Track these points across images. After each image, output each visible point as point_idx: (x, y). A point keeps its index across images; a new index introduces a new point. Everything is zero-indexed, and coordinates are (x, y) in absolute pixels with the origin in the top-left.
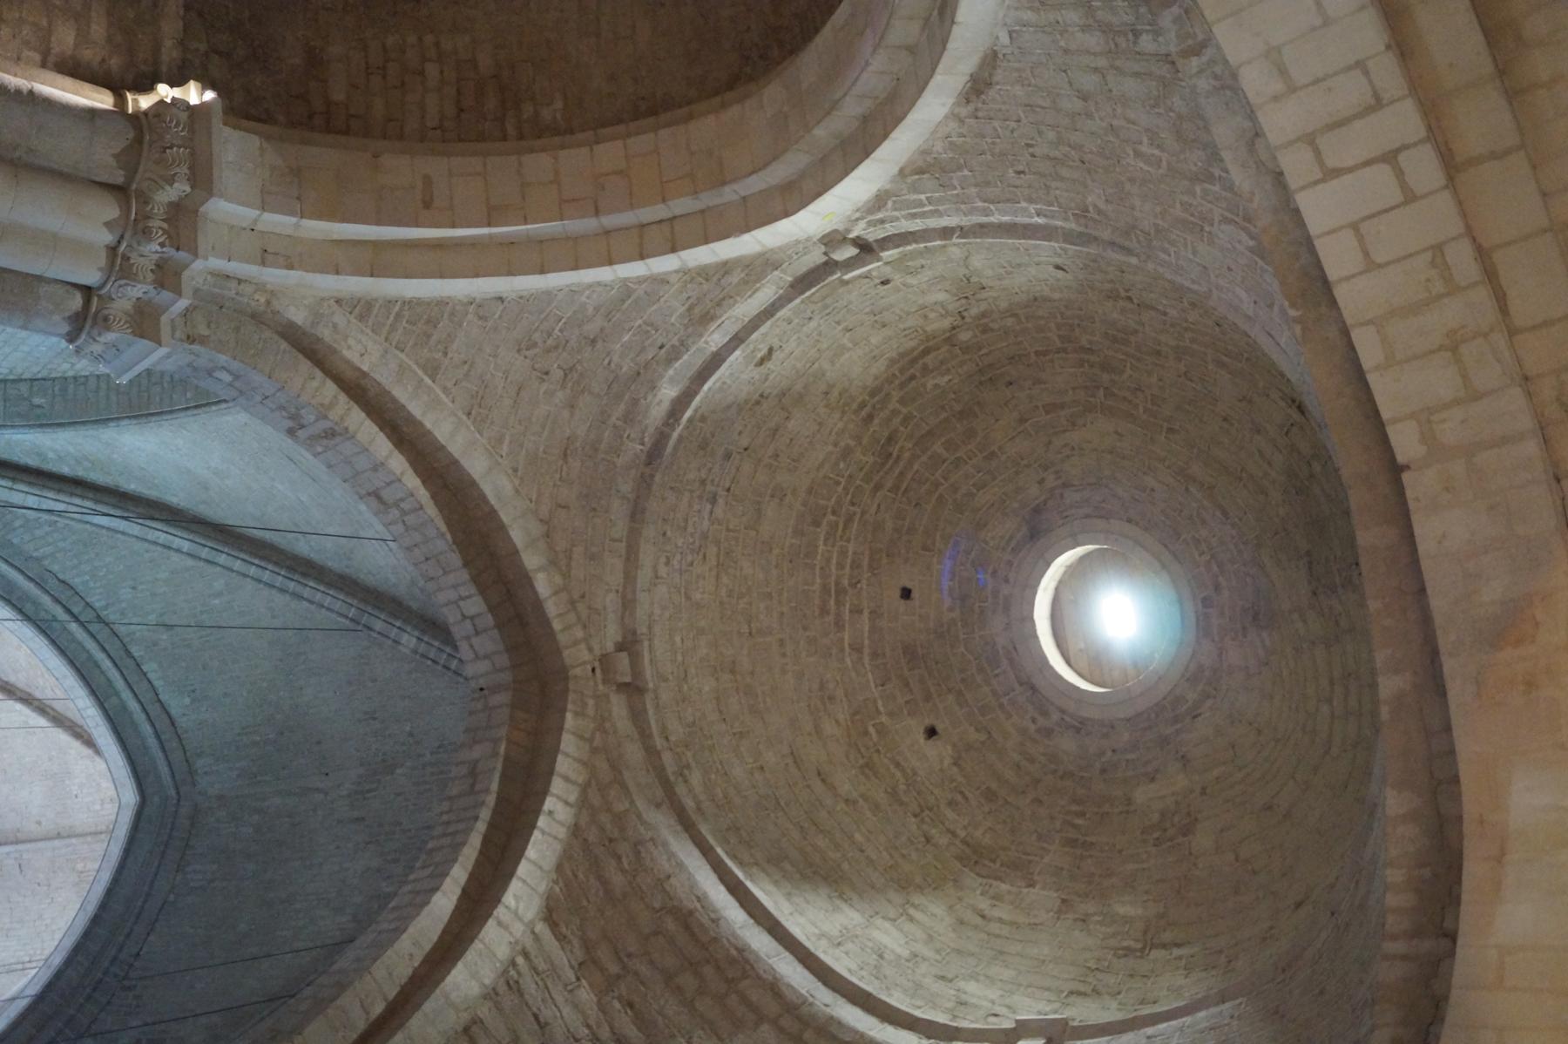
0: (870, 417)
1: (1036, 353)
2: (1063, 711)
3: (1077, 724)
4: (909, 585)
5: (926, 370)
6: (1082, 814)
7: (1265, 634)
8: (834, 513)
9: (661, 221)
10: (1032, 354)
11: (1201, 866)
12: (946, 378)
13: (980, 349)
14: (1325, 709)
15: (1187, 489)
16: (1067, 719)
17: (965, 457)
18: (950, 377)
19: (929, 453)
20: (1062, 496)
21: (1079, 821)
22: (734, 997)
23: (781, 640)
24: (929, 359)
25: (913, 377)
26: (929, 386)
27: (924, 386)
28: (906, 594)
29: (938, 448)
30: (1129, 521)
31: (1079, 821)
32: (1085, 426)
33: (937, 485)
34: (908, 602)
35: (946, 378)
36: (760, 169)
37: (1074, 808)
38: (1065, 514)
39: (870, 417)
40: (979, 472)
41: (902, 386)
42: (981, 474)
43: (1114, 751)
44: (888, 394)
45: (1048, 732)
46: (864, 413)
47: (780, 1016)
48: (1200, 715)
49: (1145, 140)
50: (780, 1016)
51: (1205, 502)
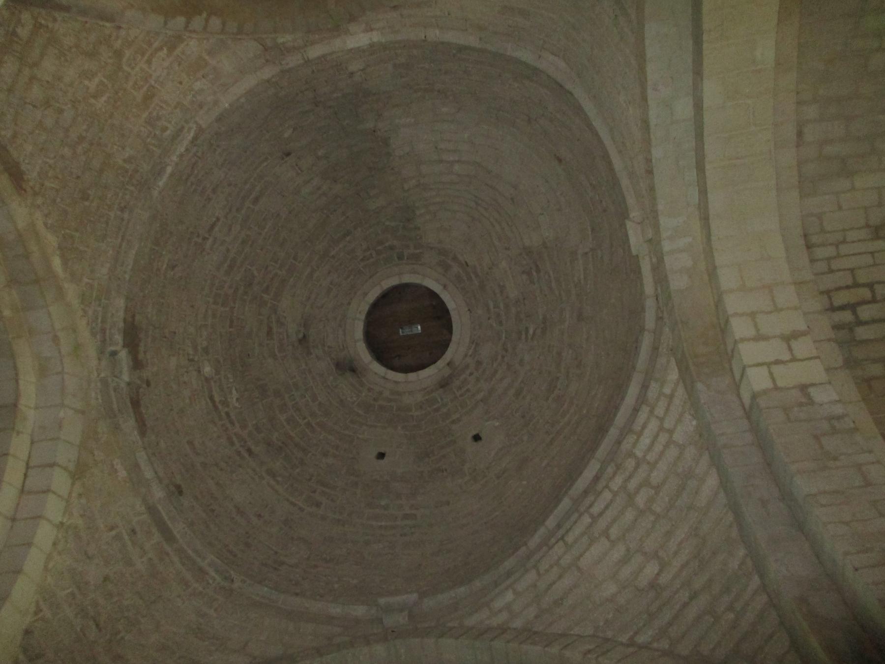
0: (249, 451)
1: (231, 327)
2: (466, 355)
3: (473, 346)
4: (375, 453)
5: (225, 403)
6: (527, 329)
7: (418, 213)
8: (314, 492)
9: (25, 475)
10: (231, 330)
11: (547, 234)
12: (234, 392)
13: (219, 362)
14: (457, 167)
15: (333, 257)
16: (470, 352)
17: (293, 403)
18: (234, 389)
19: (285, 423)
20: (329, 347)
21: (531, 331)
22: (648, 458)
23: (401, 535)
24: (217, 399)
25: (227, 414)
26: (237, 405)
27: (235, 408)
28: (381, 456)
29: (283, 418)
30: (349, 304)
31: (531, 331)
32: (285, 318)
33: (309, 425)
34: (387, 455)
35: (234, 392)
36: (17, 374)
37: (523, 336)
38: (341, 347)
39: (249, 451)
40: (305, 397)
41: (232, 423)
42: (307, 396)
43: (489, 319)
44: (235, 434)
45: (479, 363)
46: (246, 455)
47: (657, 417)
48: (466, 262)
49: (86, 82)
50: (657, 417)
51: (341, 246)
